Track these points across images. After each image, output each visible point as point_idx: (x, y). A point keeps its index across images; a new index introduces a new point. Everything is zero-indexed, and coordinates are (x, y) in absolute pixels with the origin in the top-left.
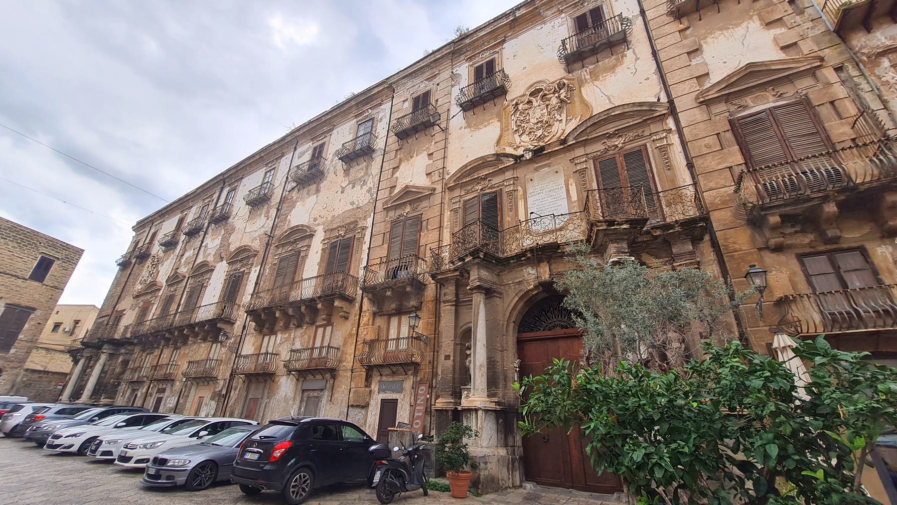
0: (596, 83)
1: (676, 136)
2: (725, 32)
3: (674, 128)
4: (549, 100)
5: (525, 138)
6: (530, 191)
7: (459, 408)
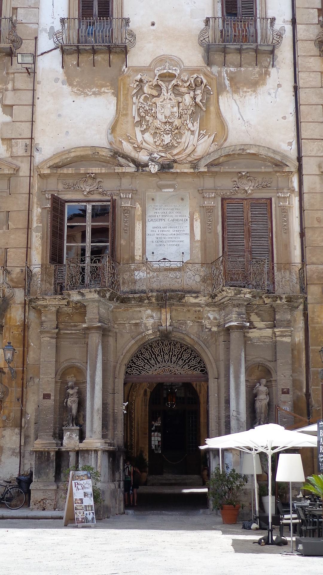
0: (236, 96)
3: (297, 189)
4: (181, 95)
6: (150, 213)
7: (63, 449)
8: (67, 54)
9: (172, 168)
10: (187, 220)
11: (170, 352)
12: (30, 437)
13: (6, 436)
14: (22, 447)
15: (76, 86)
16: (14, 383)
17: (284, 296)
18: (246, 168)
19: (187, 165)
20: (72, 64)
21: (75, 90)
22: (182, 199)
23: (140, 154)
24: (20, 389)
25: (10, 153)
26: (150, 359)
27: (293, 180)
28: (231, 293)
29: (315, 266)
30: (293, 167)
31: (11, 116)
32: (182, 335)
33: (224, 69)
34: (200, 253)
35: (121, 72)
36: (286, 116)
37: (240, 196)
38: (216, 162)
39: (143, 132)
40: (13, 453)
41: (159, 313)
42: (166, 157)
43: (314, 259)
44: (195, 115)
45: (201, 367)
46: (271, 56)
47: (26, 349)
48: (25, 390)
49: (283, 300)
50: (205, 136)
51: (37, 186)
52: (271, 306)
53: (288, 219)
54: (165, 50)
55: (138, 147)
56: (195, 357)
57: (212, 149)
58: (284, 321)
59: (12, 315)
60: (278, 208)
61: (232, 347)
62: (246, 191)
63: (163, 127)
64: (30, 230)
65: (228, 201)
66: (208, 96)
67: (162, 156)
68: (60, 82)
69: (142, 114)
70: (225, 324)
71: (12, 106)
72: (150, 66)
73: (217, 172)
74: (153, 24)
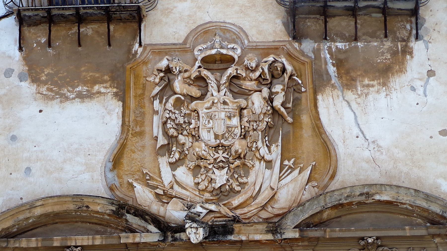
0: (350, 95)
5: (183, 174)
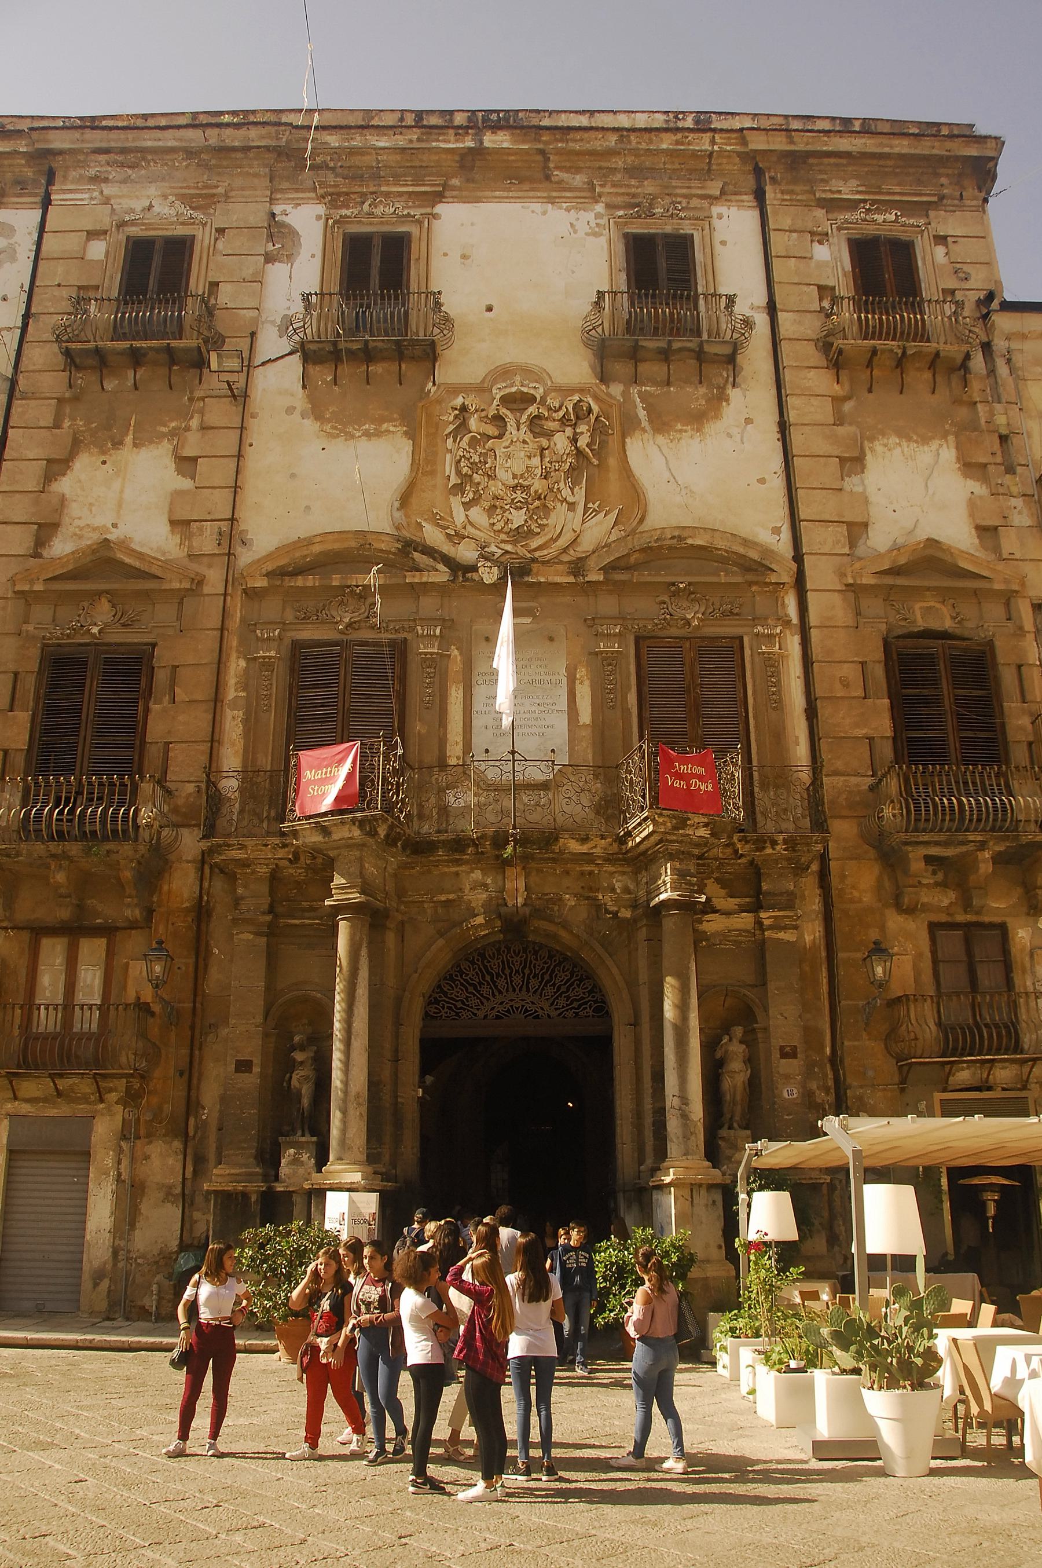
0: (660, 439)
1: (797, 639)
2: (905, 444)
4: (549, 435)
5: (477, 514)
7: (280, 1188)
8: (315, 363)
9: (528, 574)
10: (561, 681)
11: (524, 967)
12: (208, 1160)
13: (153, 1156)
14: (189, 1183)
15: (329, 421)
16: (173, 1035)
17: (780, 838)
18: (685, 575)
19: (560, 567)
20: (324, 381)
21: (328, 427)
22: (551, 639)
23: (461, 547)
24: (184, 1052)
25: (186, 550)
26: (480, 983)
27: (786, 602)
28: (664, 823)
29: (842, 778)
30: (785, 574)
31: (193, 478)
32: (551, 928)
33: (634, 391)
34: (590, 751)
35: (424, 395)
36: (766, 477)
37: (674, 631)
38: (622, 563)
39: (467, 506)
40: (168, 1195)
41: (500, 878)
42: (517, 554)
43: (839, 765)
44: (576, 473)
45: (596, 1002)
46: (731, 367)
47: (201, 960)
48: (197, 1052)
49: (778, 847)
50: (598, 512)
51: (239, 615)
52: (752, 863)
53: (779, 681)
54: (513, 352)
55: (457, 534)
56: (581, 980)
57: (613, 538)
58: (781, 894)
59: (174, 886)
60: (756, 657)
61: (667, 948)
62: (688, 623)
63: (509, 496)
64: (219, 705)
65: (648, 642)
66: (604, 437)
67: (507, 552)
68: (297, 412)
69: (465, 470)
70: (648, 901)
71: (195, 459)
72: (483, 381)
73: (624, 583)
74: (490, 309)
